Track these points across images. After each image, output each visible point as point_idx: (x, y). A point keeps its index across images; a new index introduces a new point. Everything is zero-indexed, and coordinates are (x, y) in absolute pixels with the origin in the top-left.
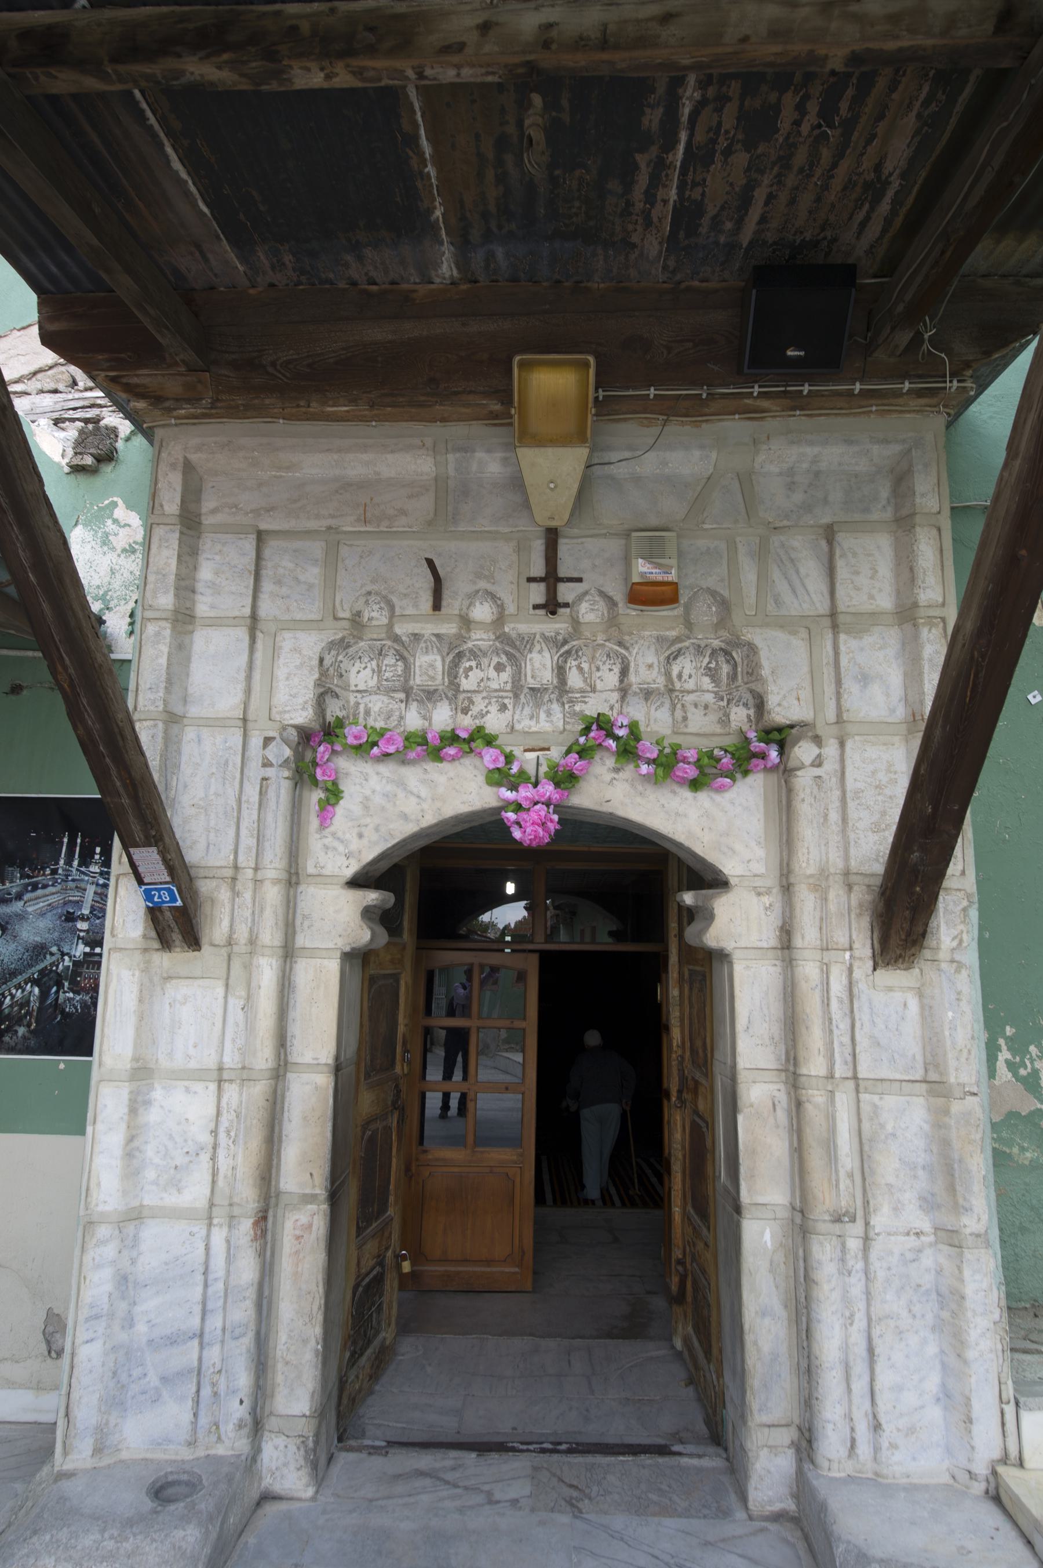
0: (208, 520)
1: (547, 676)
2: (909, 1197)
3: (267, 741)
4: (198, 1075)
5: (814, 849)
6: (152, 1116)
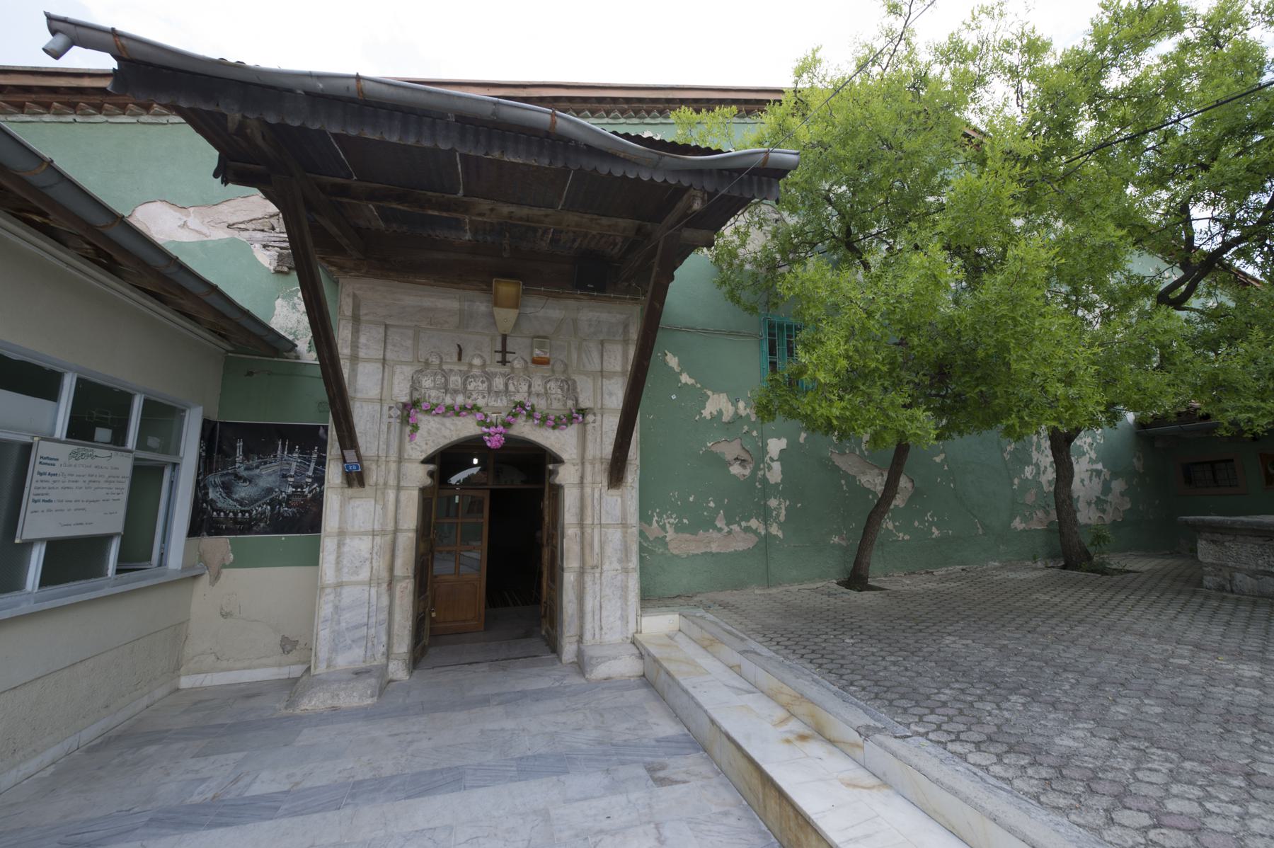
0: (363, 318)
1: (501, 387)
2: (614, 559)
3: (390, 408)
4: (365, 533)
5: (592, 451)
6: (346, 549)
